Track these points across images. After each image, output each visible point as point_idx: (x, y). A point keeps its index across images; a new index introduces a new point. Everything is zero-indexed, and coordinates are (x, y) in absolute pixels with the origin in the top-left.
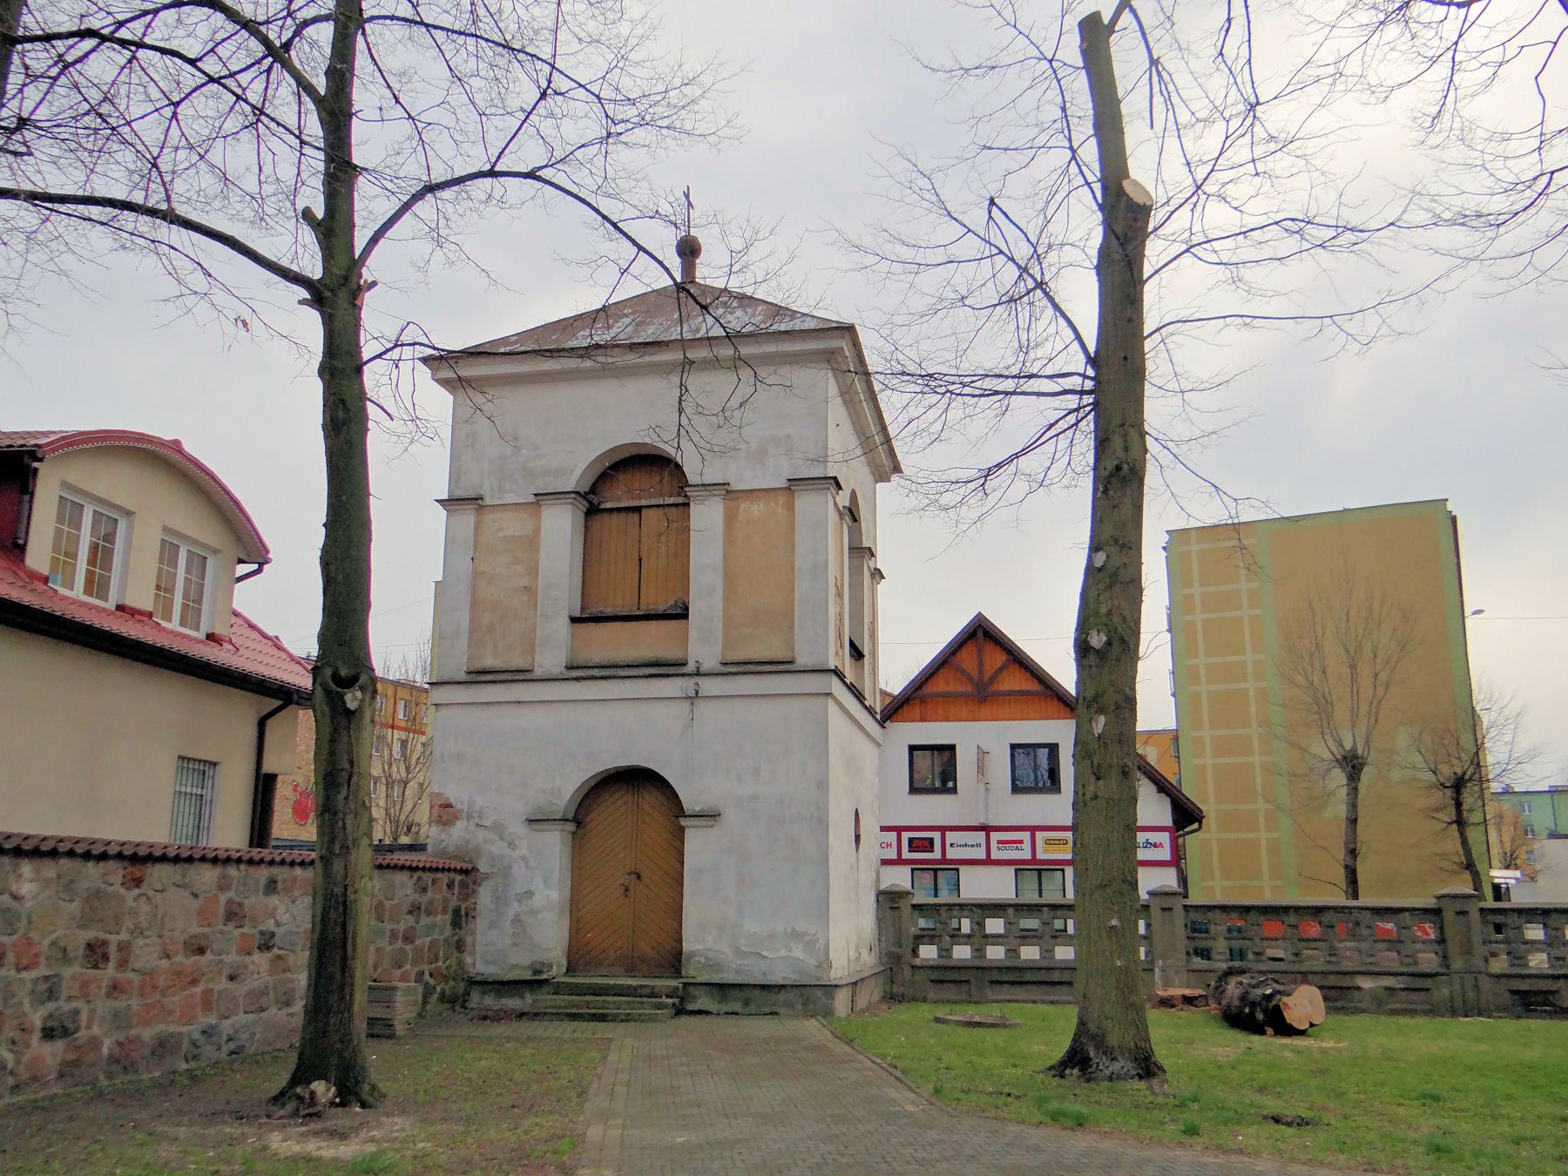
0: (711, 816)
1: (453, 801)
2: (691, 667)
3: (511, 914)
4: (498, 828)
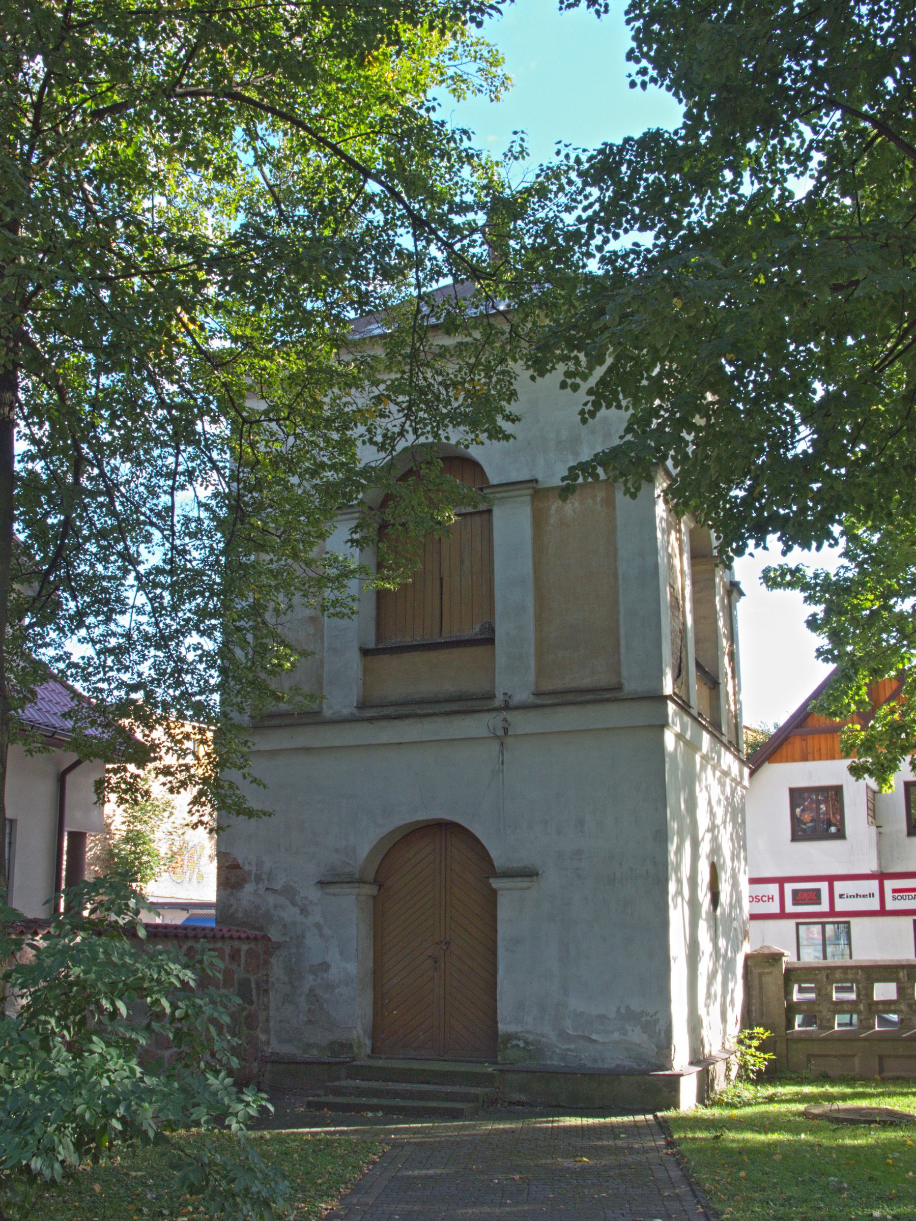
0: (530, 873)
2: (499, 701)
3: (306, 988)
4: (289, 892)
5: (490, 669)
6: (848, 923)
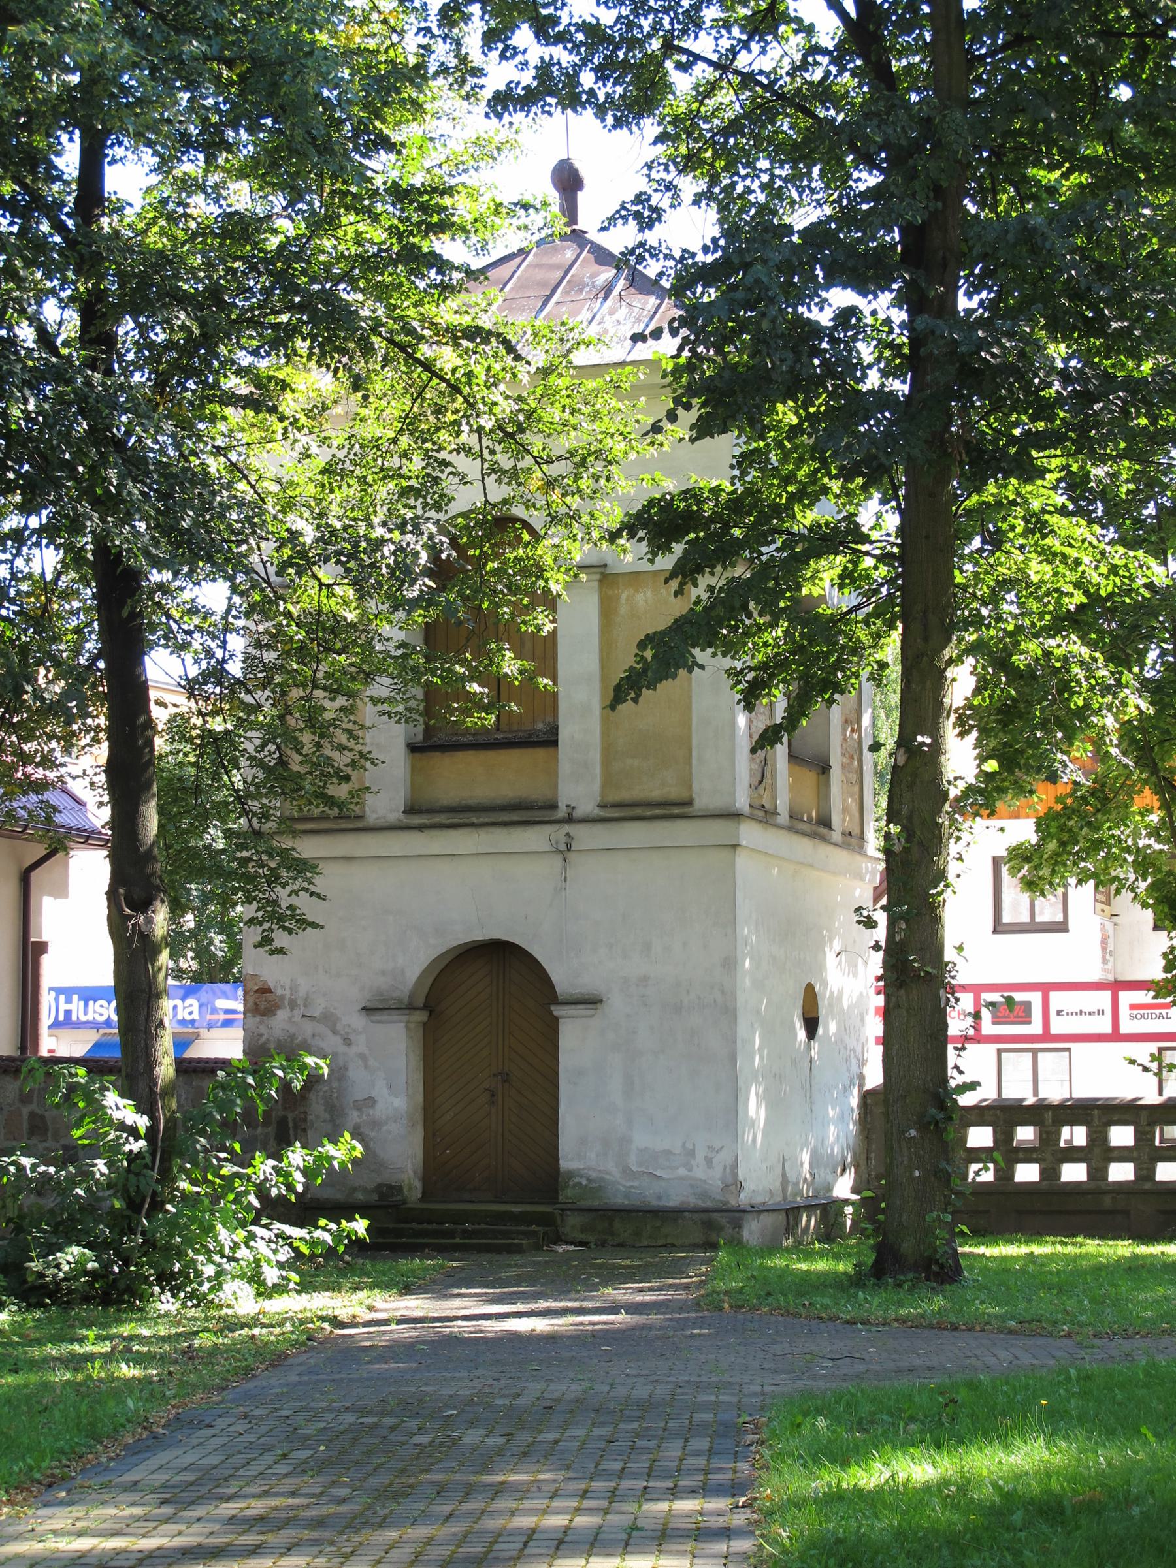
0: (592, 1001)
1: (271, 985)
5: (552, 773)
6: (1068, 1050)
